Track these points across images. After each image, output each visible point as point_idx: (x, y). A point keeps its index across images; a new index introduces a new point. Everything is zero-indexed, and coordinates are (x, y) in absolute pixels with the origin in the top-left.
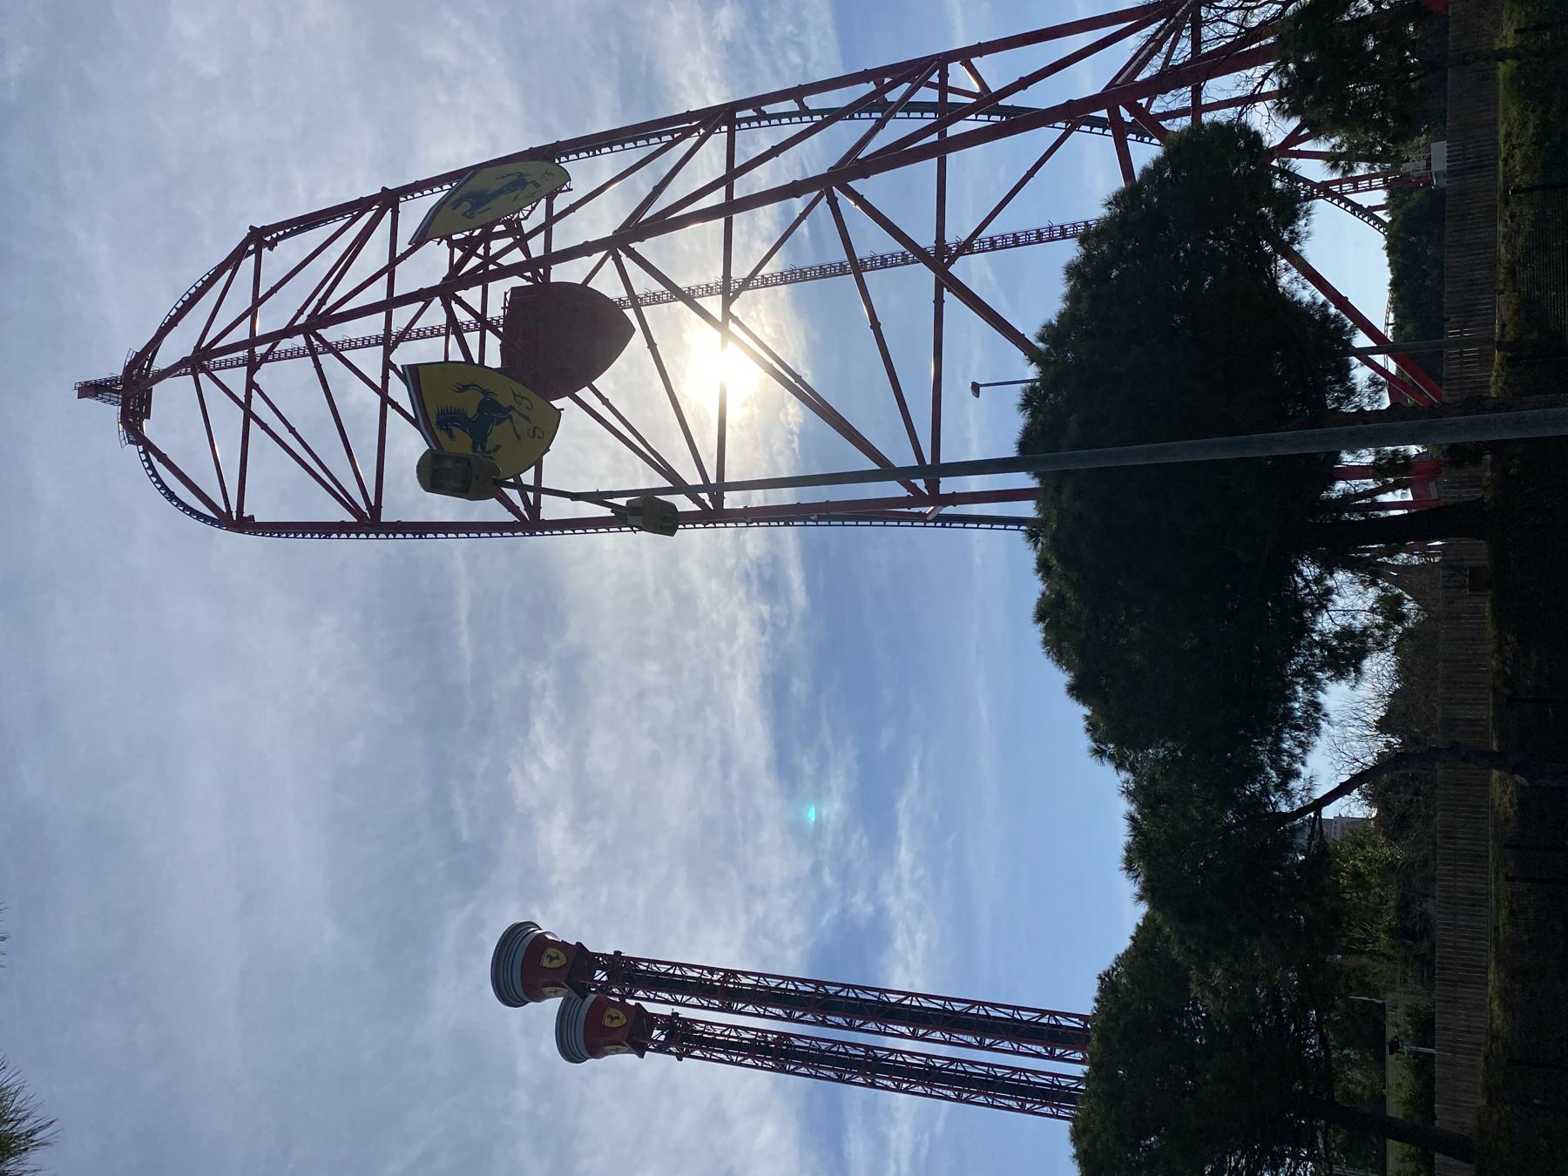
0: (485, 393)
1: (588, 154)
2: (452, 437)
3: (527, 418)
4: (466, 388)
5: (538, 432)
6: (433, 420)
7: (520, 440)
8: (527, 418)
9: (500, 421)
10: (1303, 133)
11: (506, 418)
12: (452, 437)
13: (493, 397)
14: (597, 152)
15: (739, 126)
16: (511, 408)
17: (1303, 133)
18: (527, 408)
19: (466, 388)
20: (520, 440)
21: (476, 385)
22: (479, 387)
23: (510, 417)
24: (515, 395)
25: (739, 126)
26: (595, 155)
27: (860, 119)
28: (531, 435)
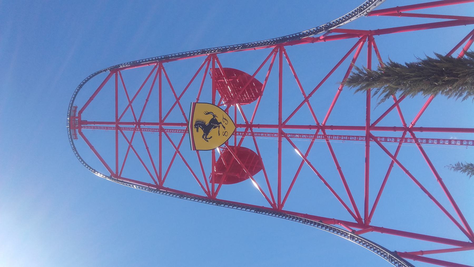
0: (214, 116)
1: (168, 56)
2: (197, 131)
3: (224, 127)
4: (209, 113)
5: (226, 134)
6: (194, 124)
7: (219, 135)
8: (224, 127)
9: (215, 127)
10: (188, 55)
11: (218, 126)
12: (197, 131)
13: (216, 118)
14: (74, 150)
15: (74, 151)
16: (221, 123)
17: (188, 55)
18: (226, 123)
19: (209, 113)
20: (219, 135)
21: (212, 113)
22: (213, 113)
23: (219, 126)
24: (223, 118)
25: (74, 151)
26: (73, 150)
27: (74, 151)
28: (223, 135)
